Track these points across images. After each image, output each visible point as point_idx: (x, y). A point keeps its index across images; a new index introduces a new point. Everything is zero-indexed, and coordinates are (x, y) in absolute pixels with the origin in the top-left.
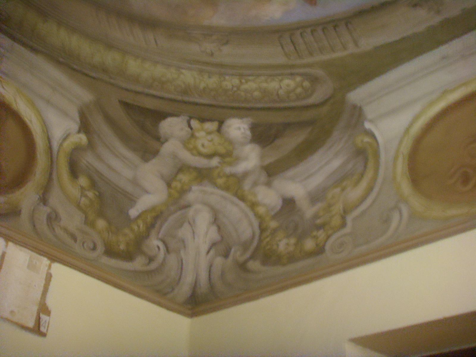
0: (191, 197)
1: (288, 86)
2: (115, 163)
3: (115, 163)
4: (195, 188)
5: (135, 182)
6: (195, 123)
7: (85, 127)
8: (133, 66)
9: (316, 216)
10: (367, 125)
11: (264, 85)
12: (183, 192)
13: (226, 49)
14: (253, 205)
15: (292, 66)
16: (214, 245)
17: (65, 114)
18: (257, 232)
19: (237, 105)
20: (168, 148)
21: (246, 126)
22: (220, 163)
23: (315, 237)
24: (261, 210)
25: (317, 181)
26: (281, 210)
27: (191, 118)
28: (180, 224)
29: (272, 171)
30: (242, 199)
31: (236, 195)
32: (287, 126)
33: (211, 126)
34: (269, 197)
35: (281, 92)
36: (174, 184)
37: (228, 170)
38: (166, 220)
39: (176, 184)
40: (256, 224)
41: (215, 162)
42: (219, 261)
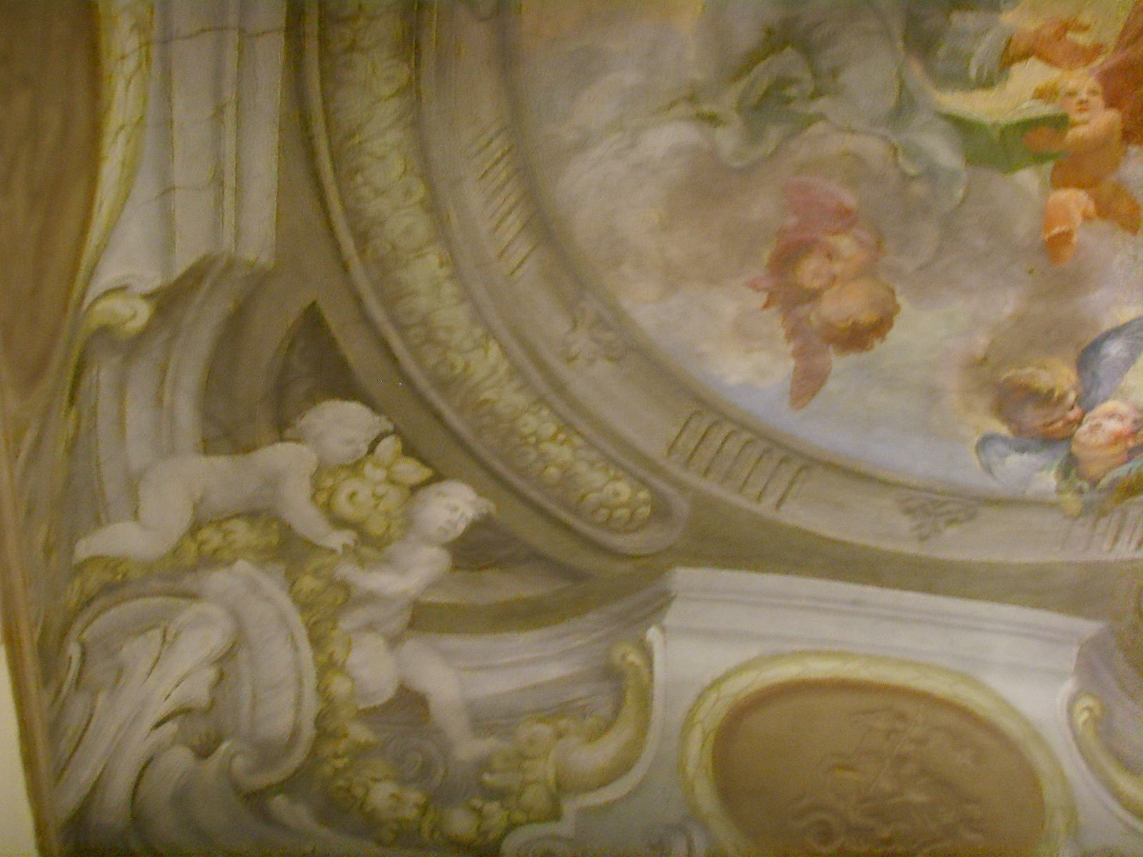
0: (218, 580)
1: (617, 494)
2: (138, 415)
3: (138, 415)
4: (242, 566)
5: (132, 484)
6: (389, 446)
7: (168, 302)
8: (425, 273)
9: (484, 765)
10: (653, 634)
11: (582, 468)
12: (210, 561)
13: (603, 368)
14: (328, 667)
15: (657, 470)
16: (183, 712)
17: (167, 246)
18: (308, 732)
19: (498, 465)
20: (280, 455)
21: (470, 513)
22: (345, 546)
23: (479, 812)
24: (340, 686)
25: (495, 685)
26: (389, 704)
27: (396, 432)
28: (141, 627)
29: (423, 618)
30: (317, 642)
31: (312, 628)
32: (536, 558)
33: (411, 471)
34: (373, 668)
35: (593, 497)
36: (206, 534)
37: (347, 570)
38: (117, 603)
39: (212, 537)
40: (311, 706)
41: (339, 539)
42: (180, 758)
